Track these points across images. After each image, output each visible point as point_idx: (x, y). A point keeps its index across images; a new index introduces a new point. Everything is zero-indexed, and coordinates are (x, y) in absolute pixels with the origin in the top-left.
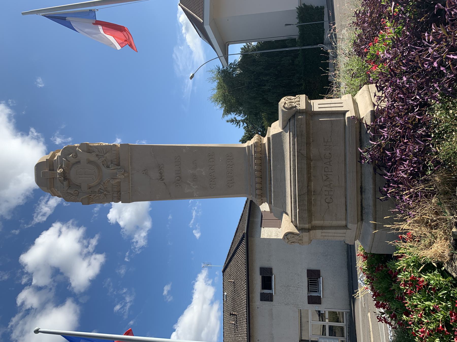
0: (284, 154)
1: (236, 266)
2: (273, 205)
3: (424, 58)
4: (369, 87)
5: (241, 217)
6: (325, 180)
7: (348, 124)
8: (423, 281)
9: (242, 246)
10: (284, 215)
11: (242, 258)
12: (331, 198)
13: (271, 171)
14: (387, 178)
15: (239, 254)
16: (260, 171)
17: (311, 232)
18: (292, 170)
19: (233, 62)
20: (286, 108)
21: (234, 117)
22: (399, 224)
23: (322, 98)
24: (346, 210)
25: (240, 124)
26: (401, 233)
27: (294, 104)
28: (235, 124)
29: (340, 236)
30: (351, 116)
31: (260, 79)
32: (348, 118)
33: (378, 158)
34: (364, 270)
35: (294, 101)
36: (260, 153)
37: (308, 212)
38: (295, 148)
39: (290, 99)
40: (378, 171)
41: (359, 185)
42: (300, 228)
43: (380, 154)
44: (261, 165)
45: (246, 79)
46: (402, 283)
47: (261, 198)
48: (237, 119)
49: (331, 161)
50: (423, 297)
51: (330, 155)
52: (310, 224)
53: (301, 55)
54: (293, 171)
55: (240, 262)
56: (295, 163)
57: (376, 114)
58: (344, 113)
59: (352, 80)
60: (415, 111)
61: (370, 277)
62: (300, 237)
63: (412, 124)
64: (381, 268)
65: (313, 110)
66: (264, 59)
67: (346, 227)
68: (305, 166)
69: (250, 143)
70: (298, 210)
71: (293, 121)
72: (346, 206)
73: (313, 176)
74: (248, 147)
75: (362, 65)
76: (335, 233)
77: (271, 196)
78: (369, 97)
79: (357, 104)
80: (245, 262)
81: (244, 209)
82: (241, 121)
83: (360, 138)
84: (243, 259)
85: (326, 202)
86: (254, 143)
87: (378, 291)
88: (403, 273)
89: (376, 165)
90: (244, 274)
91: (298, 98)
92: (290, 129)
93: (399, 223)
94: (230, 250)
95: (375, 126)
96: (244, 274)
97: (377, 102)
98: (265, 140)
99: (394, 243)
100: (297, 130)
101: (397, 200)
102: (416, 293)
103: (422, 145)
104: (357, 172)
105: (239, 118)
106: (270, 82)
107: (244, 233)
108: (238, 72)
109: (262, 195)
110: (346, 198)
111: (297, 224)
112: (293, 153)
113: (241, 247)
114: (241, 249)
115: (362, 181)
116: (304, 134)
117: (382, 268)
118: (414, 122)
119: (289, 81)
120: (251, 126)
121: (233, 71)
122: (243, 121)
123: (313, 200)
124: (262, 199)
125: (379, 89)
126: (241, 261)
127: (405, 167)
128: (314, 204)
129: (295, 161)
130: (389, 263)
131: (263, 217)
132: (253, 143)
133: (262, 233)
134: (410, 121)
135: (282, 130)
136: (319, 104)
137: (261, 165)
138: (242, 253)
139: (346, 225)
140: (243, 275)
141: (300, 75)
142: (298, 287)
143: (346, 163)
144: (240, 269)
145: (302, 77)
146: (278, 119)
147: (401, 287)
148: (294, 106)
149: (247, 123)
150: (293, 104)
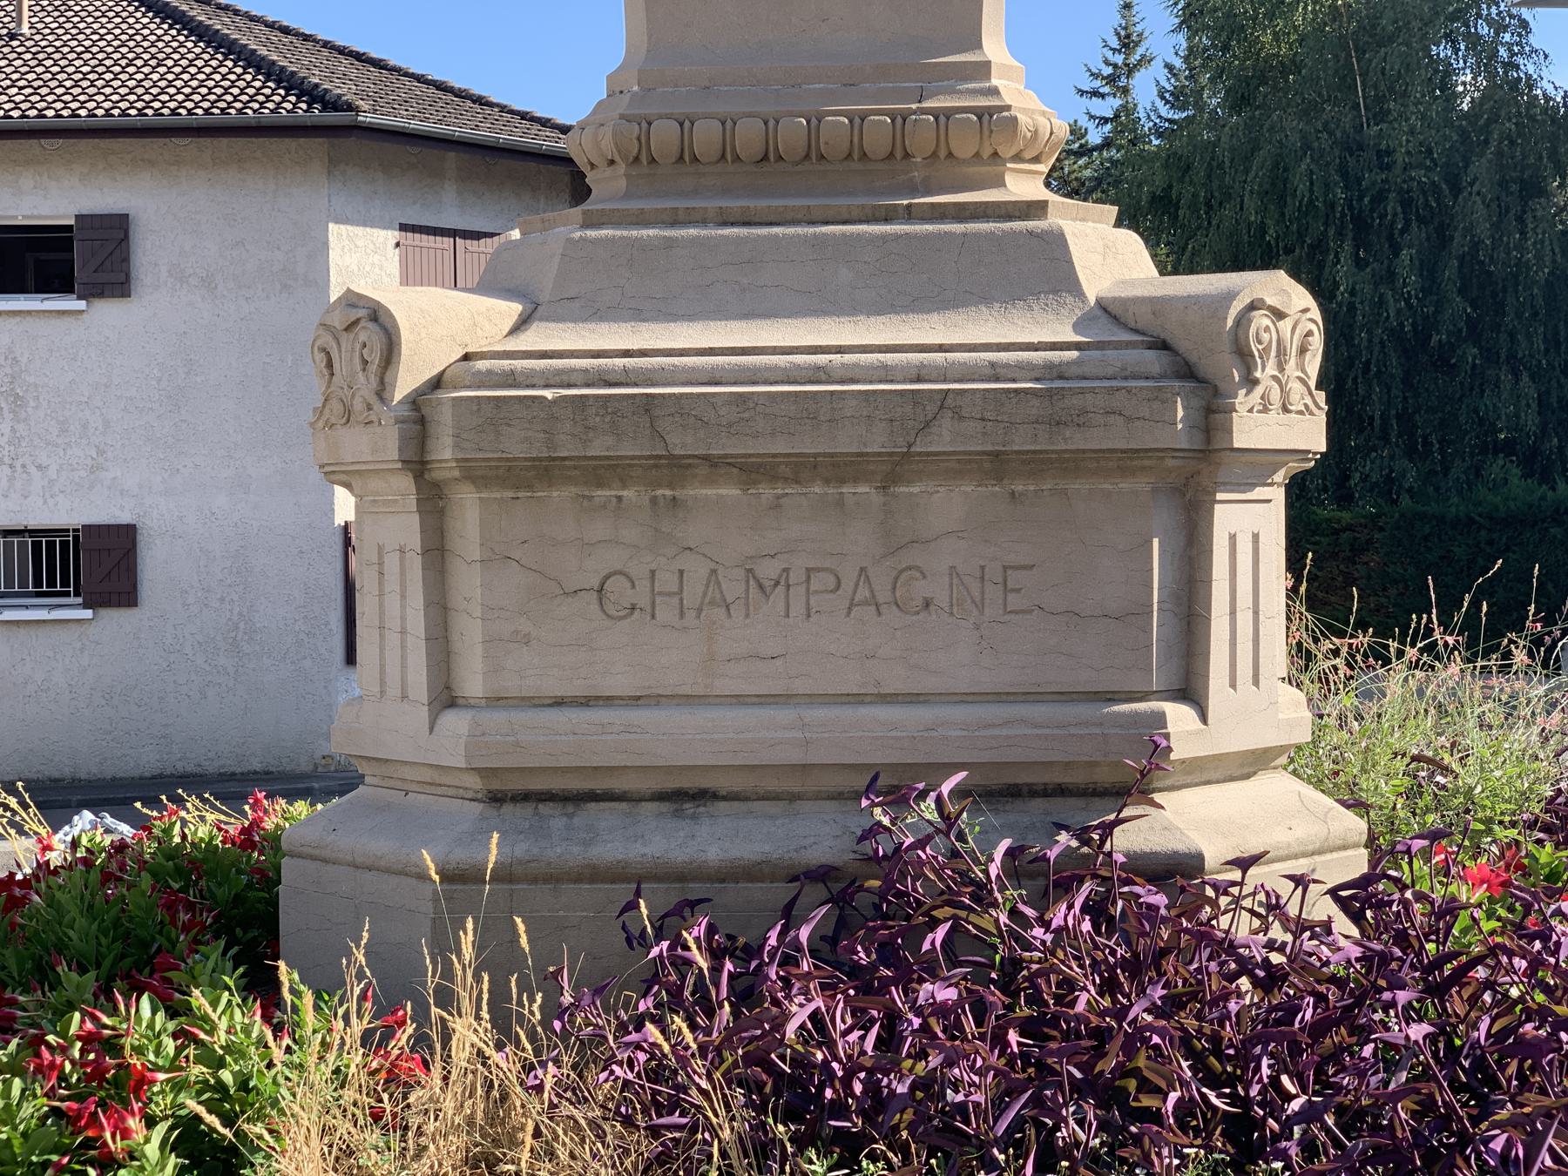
0: (929, 311)
1: (124, 50)
2: (577, 235)
3: (1550, 1140)
4: (1350, 852)
5: (462, 94)
6: (750, 571)
7: (1119, 714)
8: (126, 1133)
9: (267, 91)
10: (512, 310)
11: (187, 90)
12: (633, 608)
13: (812, 223)
14: (773, 941)
15: (208, 70)
16: (813, 154)
17: (406, 483)
18: (822, 359)
19: (1535, 40)
20: (1243, 320)
21: (1154, 51)
22: (479, 1008)
23: (1294, 564)
24: (559, 703)
25: (1103, 96)
26: (421, 1016)
27: (1265, 373)
28: (1107, 63)
29: (382, 667)
30: (1167, 736)
31: (1407, 222)
32: (1160, 719)
33: (900, 895)
34: (164, 831)
35: (1287, 372)
36: (935, 155)
37: (540, 459)
38: (973, 381)
39: (1303, 350)
40: (816, 891)
41: (721, 783)
42: (426, 411)
43: (919, 903)
44: (857, 154)
45: (1412, 132)
46: (106, 1020)
47: (624, 158)
48: (1137, 75)
49: (879, 614)
50: (24, 1135)
51: (919, 602)
52: (456, 473)
53: (1543, 498)
54: (818, 368)
55: (155, 77)
56: (871, 382)
57: (1180, 881)
58: (1190, 692)
59: (1396, 754)
60: (1204, 1090)
61: (122, 867)
62: (369, 408)
63: (1123, 1072)
64: (184, 917)
65: (1220, 496)
66: (1539, 257)
67: (446, 698)
68: (845, 443)
69: (1012, 85)
70: (549, 394)
71: (1156, 369)
72: (586, 702)
73: (778, 497)
74: (984, 69)
75: (1488, 821)
76: (403, 632)
77: (641, 220)
78: (1289, 845)
79: (1247, 777)
80: (157, 113)
81: (524, 116)
82: (1124, 107)
83: (1025, 790)
84: (180, 97)
85: (607, 577)
86: (1008, 108)
87: (36, 898)
88: (171, 1026)
89: (853, 882)
90: (74, 105)
91: (1308, 401)
92: (1099, 346)
93: (485, 1007)
94: (236, 12)
95: (1104, 879)
96: (74, 105)
97: (1254, 894)
98: (1024, 185)
99: (360, 976)
100: (1092, 390)
101: (628, 999)
102: (46, 1095)
103: (992, 1129)
104: (805, 768)
105: (1146, 91)
106: (1381, 295)
107: (357, 110)
108: (1467, 83)
109: (644, 158)
110: (635, 701)
111: (455, 388)
112: (937, 367)
113: (257, 84)
114: (242, 84)
115: (747, 799)
116: (1065, 440)
117: (186, 928)
118: (1132, 1085)
119: (1377, 422)
120: (1087, 173)
121: (1474, 41)
122: (1123, 120)
123: (619, 498)
124: (612, 162)
125: (1344, 893)
126: (163, 84)
127: (845, 1034)
128: (590, 498)
129: (880, 382)
130: (224, 954)
131: (472, 245)
132: (1009, 102)
133: (359, 230)
134: (1141, 1061)
135: (1092, 301)
136: (1256, 537)
137: (857, 154)
138: (219, 91)
139: (461, 701)
140: (68, 98)
141: (1409, 490)
142: (19, 469)
143: (862, 703)
144: (108, 76)
145: (1395, 502)
146: (1163, 272)
147: (77, 1016)
148: (1258, 374)
149: (1107, 144)
150: (1271, 369)
